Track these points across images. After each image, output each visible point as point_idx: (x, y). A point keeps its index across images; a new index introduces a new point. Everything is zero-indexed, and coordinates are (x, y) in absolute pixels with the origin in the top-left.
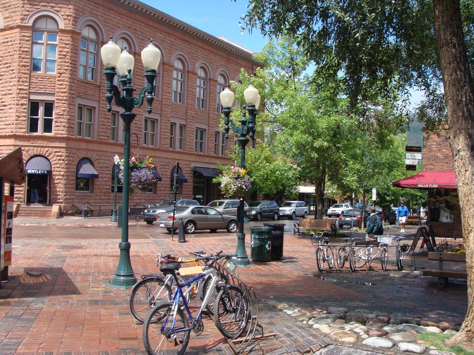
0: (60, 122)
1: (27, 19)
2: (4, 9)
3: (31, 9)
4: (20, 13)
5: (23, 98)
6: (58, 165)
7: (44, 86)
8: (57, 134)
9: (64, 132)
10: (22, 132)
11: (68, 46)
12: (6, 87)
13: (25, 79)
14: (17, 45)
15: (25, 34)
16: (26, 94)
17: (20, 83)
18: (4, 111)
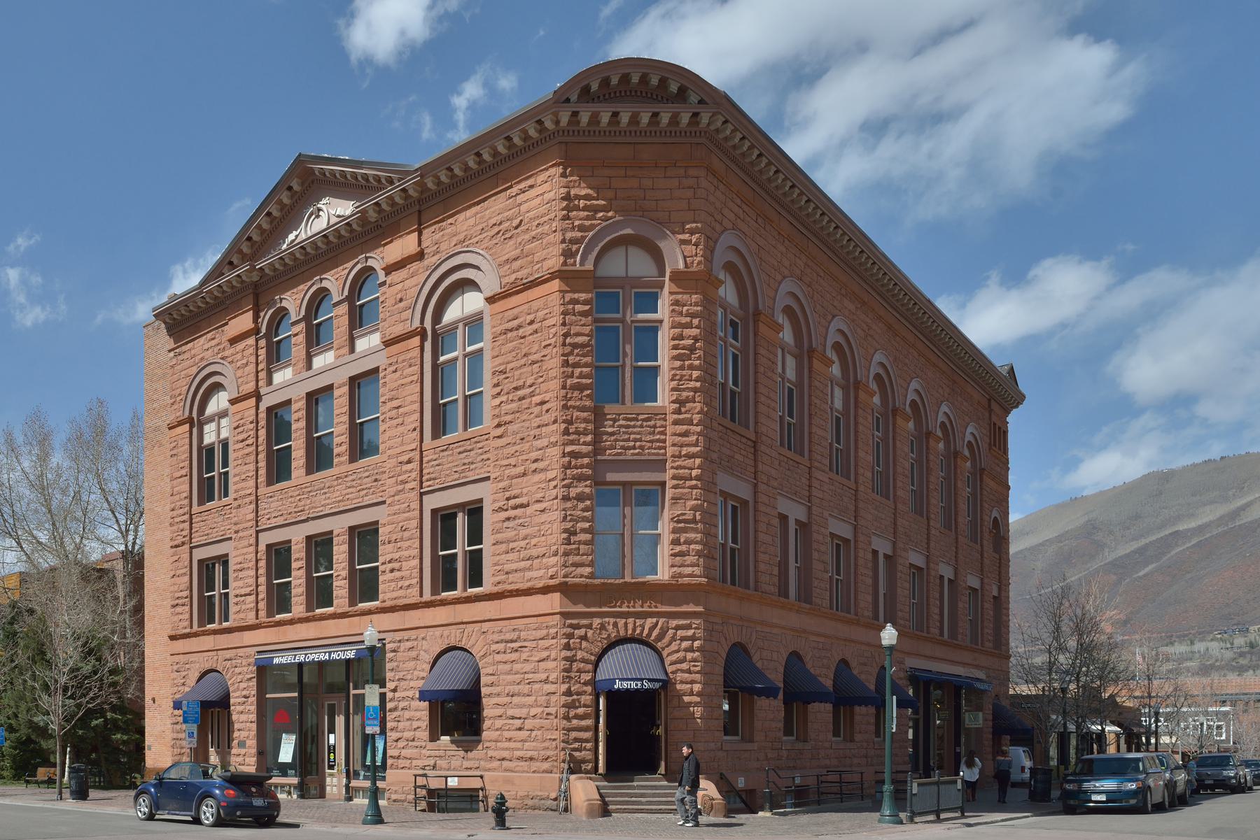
0: (685, 543)
1: (578, 251)
2: (500, 238)
3: (587, 223)
4: (559, 236)
5: (580, 478)
6: (685, 666)
7: (635, 440)
8: (681, 575)
9: (697, 571)
10: (582, 576)
11: (696, 322)
12: (522, 453)
13: (583, 425)
14: (553, 330)
15: (576, 296)
16: (587, 466)
17: (571, 437)
18: (517, 521)
